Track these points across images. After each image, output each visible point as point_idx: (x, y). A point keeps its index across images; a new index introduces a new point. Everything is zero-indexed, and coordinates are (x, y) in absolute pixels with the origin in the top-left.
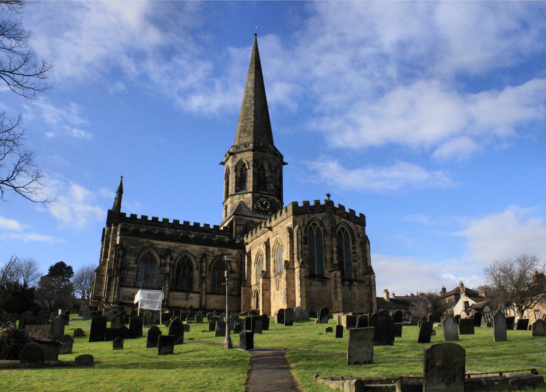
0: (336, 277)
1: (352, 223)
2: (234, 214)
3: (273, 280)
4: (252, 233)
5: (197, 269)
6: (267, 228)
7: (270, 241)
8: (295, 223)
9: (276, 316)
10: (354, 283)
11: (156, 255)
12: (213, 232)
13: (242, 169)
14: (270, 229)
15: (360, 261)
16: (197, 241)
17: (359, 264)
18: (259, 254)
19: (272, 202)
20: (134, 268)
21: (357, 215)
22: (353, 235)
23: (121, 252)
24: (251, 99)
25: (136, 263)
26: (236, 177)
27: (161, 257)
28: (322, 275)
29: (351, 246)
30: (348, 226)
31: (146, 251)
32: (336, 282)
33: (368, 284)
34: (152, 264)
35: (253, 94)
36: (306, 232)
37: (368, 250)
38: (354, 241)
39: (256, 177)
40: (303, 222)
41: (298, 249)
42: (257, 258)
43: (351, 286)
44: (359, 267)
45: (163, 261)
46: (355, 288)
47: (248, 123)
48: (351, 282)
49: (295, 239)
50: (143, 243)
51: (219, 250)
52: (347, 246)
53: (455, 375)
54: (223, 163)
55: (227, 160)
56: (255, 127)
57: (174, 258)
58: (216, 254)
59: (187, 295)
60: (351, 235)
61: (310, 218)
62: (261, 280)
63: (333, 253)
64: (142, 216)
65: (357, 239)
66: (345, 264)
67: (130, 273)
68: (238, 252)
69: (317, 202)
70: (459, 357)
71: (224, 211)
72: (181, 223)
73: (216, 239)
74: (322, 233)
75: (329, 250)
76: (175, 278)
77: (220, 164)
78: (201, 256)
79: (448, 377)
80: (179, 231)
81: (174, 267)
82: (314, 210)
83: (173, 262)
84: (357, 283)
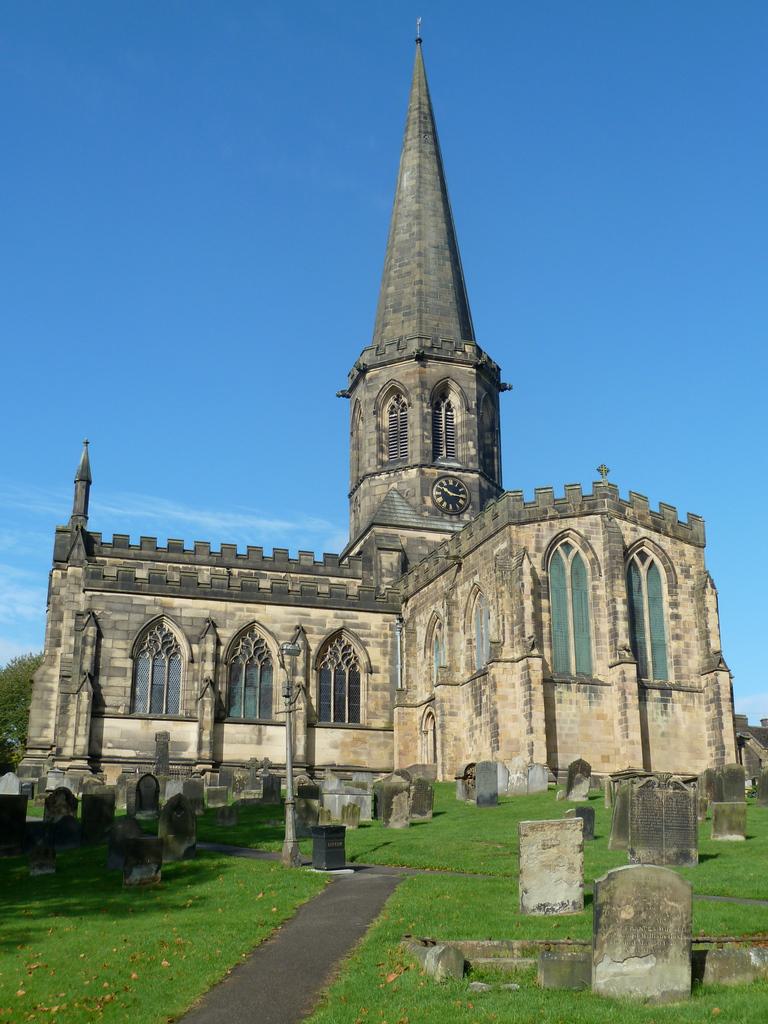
0: (624, 680)
15: (693, 637)
16: (279, 596)
17: (687, 645)
18: (435, 618)
20: (126, 669)
23: (91, 631)
28: (589, 676)
29: (666, 598)
30: (658, 547)
32: (624, 693)
33: (711, 696)
38: (673, 586)
39: (429, 426)
42: (430, 633)
43: (667, 701)
44: (687, 652)
45: (196, 648)
46: (678, 707)
47: (405, 286)
51: (336, 616)
52: (656, 600)
53: (667, 941)
58: (328, 626)
59: (260, 731)
60: (667, 570)
63: (616, 618)
67: (117, 681)
70: (676, 901)
73: (325, 589)
74: (588, 567)
75: (604, 610)
77: (339, 396)
78: (291, 634)
79: (651, 946)
80: (235, 571)
82: (565, 511)
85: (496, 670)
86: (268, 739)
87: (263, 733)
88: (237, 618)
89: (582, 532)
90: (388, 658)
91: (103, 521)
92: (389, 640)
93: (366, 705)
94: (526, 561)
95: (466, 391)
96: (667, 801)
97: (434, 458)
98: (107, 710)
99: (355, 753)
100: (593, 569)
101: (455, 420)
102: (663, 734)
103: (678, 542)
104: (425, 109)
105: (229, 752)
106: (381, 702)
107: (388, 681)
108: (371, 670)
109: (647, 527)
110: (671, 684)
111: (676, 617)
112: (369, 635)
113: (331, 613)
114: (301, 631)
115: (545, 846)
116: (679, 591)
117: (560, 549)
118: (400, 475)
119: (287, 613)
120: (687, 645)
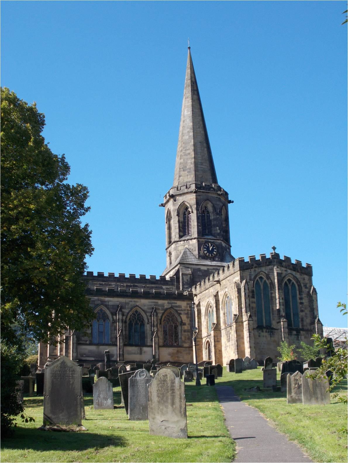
1: (298, 274)
2: (179, 263)
3: (223, 332)
4: (200, 284)
6: (215, 281)
7: (219, 294)
8: (242, 279)
9: (228, 365)
10: (301, 332)
11: (108, 312)
12: (159, 283)
13: (185, 212)
14: (218, 282)
15: (307, 311)
16: (146, 295)
17: (306, 314)
18: (209, 306)
19: (219, 247)
21: (304, 265)
22: (299, 286)
24: (189, 130)
26: (179, 221)
29: (298, 296)
30: (295, 277)
31: (168, 311)
34: (104, 321)
35: (191, 124)
37: (315, 300)
38: (301, 292)
39: (200, 221)
40: (250, 277)
41: (246, 303)
42: (207, 309)
44: (306, 317)
45: (114, 317)
48: (298, 331)
49: (243, 294)
50: (94, 301)
51: (168, 303)
52: (294, 297)
54: (163, 205)
55: (168, 201)
56: (196, 164)
57: (126, 314)
58: (165, 307)
59: (141, 349)
60: (298, 286)
62: (212, 333)
65: (304, 289)
66: (292, 314)
68: (187, 304)
69: (263, 257)
71: (168, 258)
72: (127, 276)
74: (269, 285)
76: (127, 332)
77: (160, 206)
81: (125, 322)
84: (304, 332)
86: (144, 352)
87: (142, 350)
88: (130, 305)
89: (267, 272)
90: (189, 319)
92: (189, 312)
93: (181, 338)
95: (215, 206)
99: (178, 357)
100: (271, 286)
101: (211, 218)
103: (302, 275)
104: (193, 79)
106: (187, 337)
107: (189, 328)
109: (290, 269)
110: (300, 329)
112: (182, 310)
113: (166, 302)
115: (269, 374)
116: (303, 293)
117: (258, 279)
118: (189, 242)
119: (152, 302)
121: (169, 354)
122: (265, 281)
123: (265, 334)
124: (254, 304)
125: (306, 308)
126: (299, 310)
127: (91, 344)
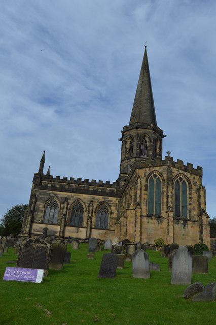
0: (169, 217)
5: (86, 211)
10: (188, 222)
15: (196, 205)
16: (87, 192)
17: (194, 207)
20: (42, 210)
22: (190, 183)
23: (34, 200)
25: (44, 207)
27: (61, 203)
28: (159, 215)
29: (188, 192)
30: (185, 177)
36: (147, 181)
38: (190, 188)
45: (62, 205)
46: (189, 226)
48: (185, 221)
51: (103, 198)
52: (184, 192)
61: (179, 173)
64: (106, 182)
65: (193, 186)
66: (181, 206)
74: (162, 182)
80: (81, 186)
81: (70, 209)
82: (155, 164)
83: (69, 206)
84: (191, 222)
85: (128, 212)
91: (57, 170)
94: (139, 179)
96: (37, 248)
97: (140, 155)
98: (35, 221)
99: (105, 237)
102: (183, 235)
105: (67, 234)
108: (111, 213)
111: (190, 198)
113: (101, 197)
114: (92, 201)
120: (194, 207)
121: (99, 235)
122: (158, 178)
123: (153, 221)
124: (146, 196)
125: (194, 202)
126: (188, 203)
127: (42, 223)
